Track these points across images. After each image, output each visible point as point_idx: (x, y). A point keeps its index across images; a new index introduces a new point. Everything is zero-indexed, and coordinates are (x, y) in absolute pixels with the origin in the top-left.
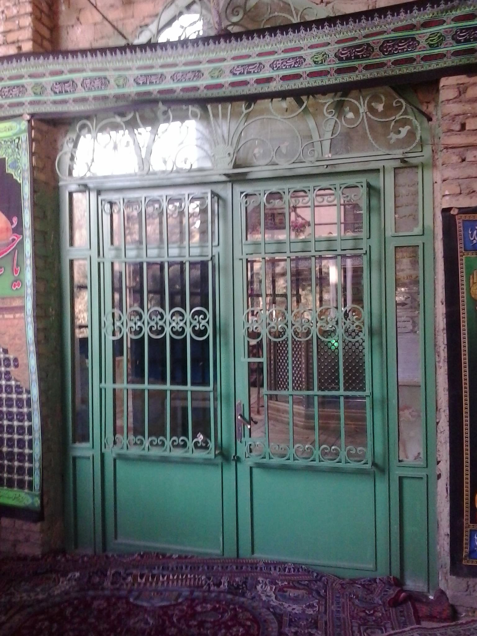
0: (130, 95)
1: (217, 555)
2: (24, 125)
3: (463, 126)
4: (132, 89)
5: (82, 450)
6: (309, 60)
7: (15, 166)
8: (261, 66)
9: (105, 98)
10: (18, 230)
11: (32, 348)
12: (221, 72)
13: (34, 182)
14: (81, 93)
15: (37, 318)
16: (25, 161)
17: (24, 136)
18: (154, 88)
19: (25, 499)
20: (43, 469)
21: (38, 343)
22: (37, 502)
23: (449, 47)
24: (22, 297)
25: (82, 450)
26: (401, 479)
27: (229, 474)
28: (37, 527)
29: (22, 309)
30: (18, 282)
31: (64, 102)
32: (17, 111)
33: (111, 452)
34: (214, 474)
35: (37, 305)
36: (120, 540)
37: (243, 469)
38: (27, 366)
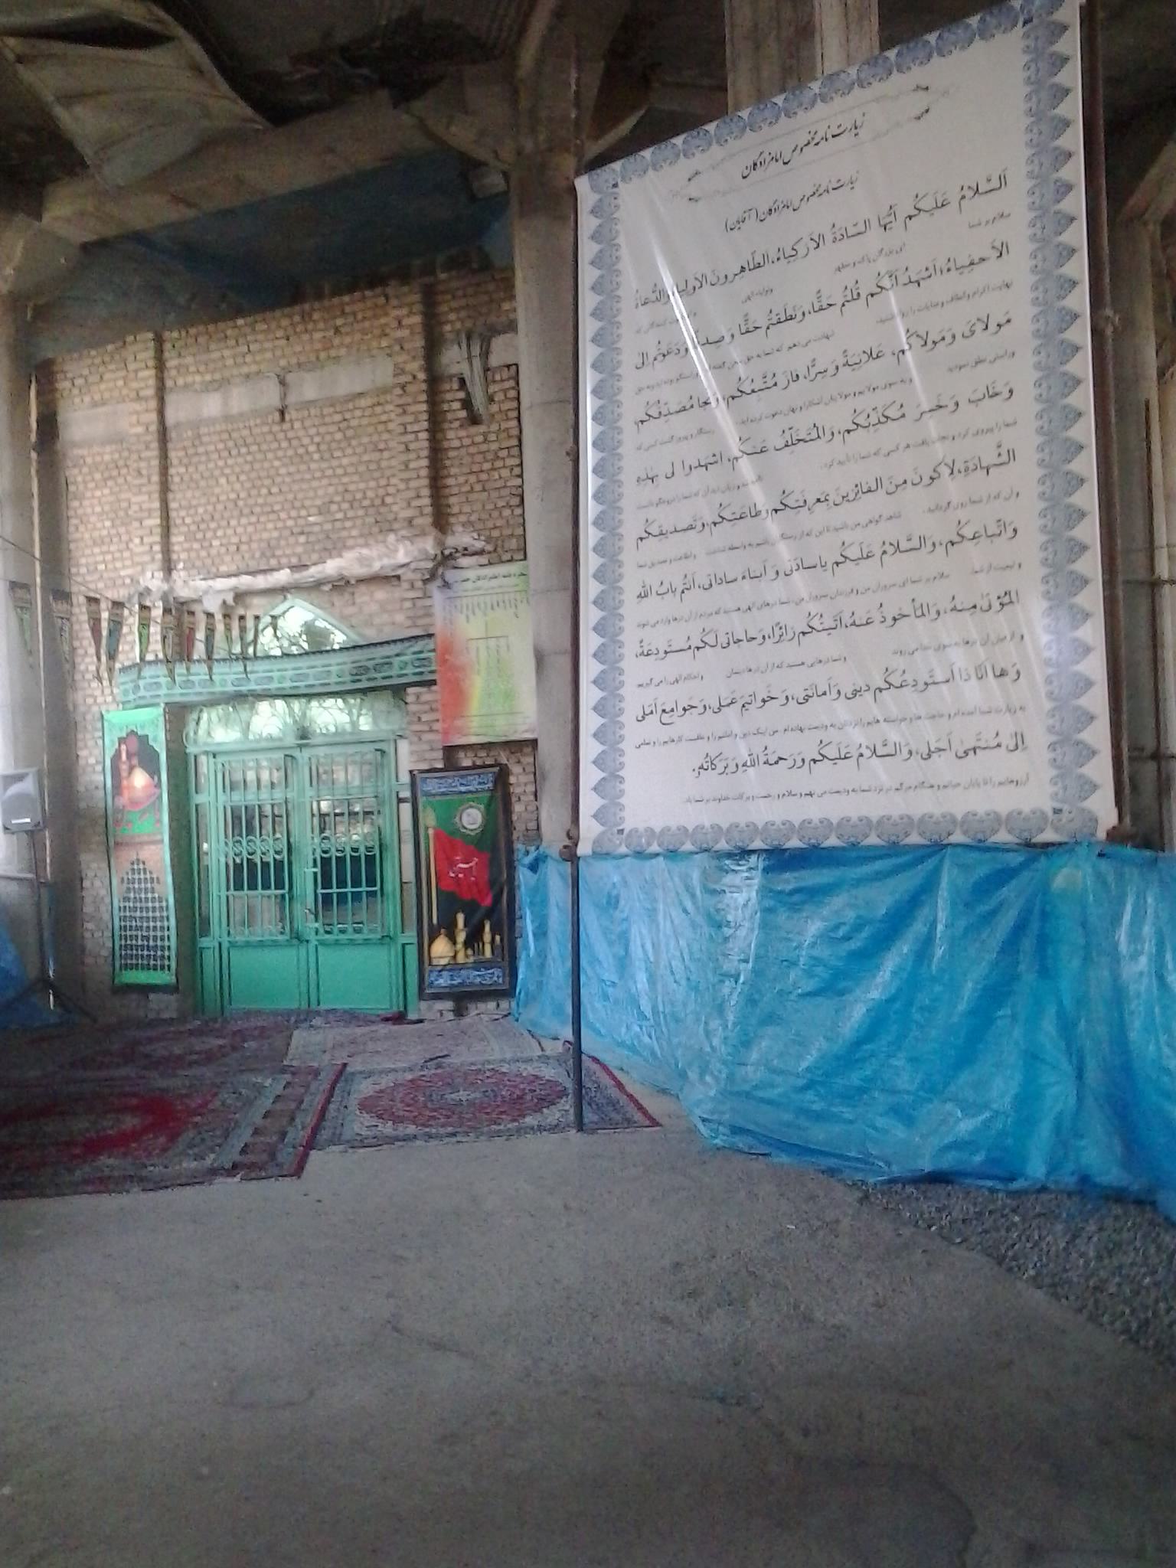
0: (1020, 813)
1: (235, 742)
2: (161, 710)
3: (419, 719)
4: (230, 689)
5: (204, 942)
6: (334, 675)
7: (155, 740)
8: (306, 676)
9: (213, 693)
10: (159, 785)
11: (169, 870)
12: (284, 677)
13: (168, 750)
14: (198, 689)
15: (171, 849)
16: (162, 736)
17: (162, 719)
18: (244, 689)
19: (165, 978)
20: (177, 956)
21: (173, 866)
22: (173, 979)
23: (409, 670)
24: (162, 834)
25: (204, 942)
26: (404, 945)
27: (303, 951)
28: (173, 998)
29: (162, 841)
30: (159, 821)
31: (421, 673)
32: (157, 700)
33: (225, 940)
34: (292, 952)
35: (171, 838)
36: (234, 1006)
37: (312, 946)
38: (166, 883)
